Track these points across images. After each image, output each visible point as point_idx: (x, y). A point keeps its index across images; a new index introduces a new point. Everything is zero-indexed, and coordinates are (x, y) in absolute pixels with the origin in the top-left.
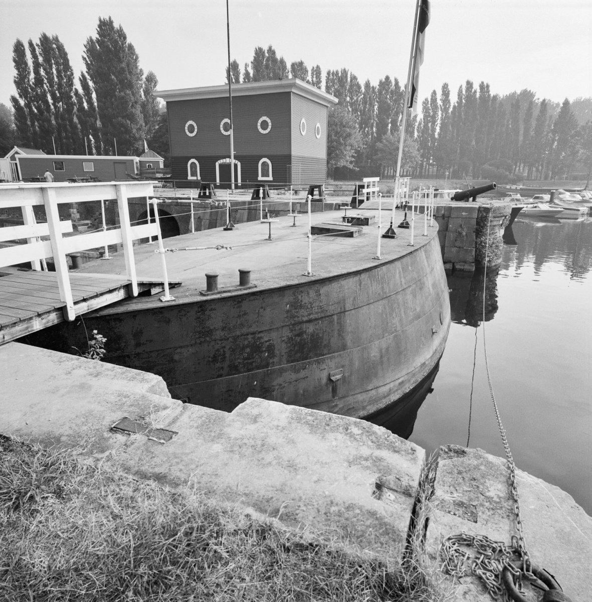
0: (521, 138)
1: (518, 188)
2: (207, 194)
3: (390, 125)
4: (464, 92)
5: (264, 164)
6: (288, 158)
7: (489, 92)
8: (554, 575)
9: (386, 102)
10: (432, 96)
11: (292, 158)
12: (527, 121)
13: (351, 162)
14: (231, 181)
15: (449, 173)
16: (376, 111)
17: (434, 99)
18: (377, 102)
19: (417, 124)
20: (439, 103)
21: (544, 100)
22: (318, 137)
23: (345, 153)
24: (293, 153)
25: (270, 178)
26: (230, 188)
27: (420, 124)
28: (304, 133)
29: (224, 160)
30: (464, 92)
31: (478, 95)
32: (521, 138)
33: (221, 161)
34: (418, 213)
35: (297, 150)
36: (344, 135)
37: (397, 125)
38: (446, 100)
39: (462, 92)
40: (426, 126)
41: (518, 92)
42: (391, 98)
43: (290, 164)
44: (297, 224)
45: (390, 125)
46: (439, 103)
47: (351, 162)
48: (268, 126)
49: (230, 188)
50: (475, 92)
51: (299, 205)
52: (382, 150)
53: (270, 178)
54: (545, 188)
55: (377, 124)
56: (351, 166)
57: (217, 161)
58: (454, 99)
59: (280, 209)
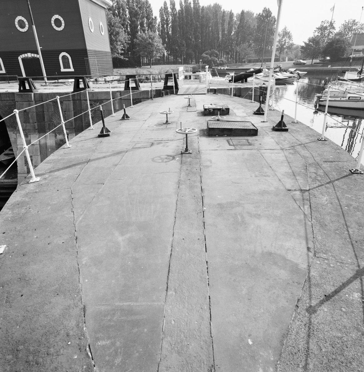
0: (220, 36)
1: (225, 69)
2: (27, 87)
3: (139, 26)
4: (183, 4)
5: (64, 57)
6: (84, 52)
7: (199, 4)
8: (166, 283)
9: (134, 9)
10: (164, 5)
11: (88, 52)
12: (223, 25)
13: (121, 54)
14: (43, 75)
15: (181, 60)
16: (128, 16)
17: (166, 8)
18: (127, 8)
19: (157, 25)
20: (170, 10)
21: (243, 12)
22: (103, 34)
23: (117, 47)
24: (88, 48)
25: (72, 70)
26: (43, 79)
27: (159, 26)
28: (92, 31)
29: (26, 55)
30: (183, 4)
31: (192, 6)
32: (220, 36)
33: (23, 56)
34: (253, 101)
35: (91, 45)
36: (114, 33)
37: (172, 28)
38: (173, 8)
39: (182, 3)
40: (163, 26)
41: (212, 5)
42: (137, 6)
43: (87, 57)
44: (169, 121)
45: (139, 26)
46: (170, 10)
47: (121, 54)
48: (61, 23)
49: (43, 79)
50: (190, 3)
51: (118, 94)
52: (139, 44)
53: (72, 70)
54: (239, 68)
55: (130, 25)
56: (122, 57)
57: (19, 55)
58: (178, 8)
59: (103, 98)
